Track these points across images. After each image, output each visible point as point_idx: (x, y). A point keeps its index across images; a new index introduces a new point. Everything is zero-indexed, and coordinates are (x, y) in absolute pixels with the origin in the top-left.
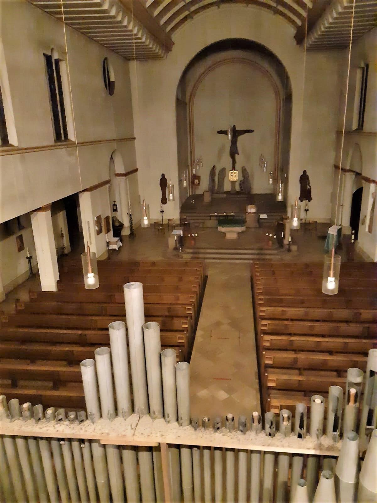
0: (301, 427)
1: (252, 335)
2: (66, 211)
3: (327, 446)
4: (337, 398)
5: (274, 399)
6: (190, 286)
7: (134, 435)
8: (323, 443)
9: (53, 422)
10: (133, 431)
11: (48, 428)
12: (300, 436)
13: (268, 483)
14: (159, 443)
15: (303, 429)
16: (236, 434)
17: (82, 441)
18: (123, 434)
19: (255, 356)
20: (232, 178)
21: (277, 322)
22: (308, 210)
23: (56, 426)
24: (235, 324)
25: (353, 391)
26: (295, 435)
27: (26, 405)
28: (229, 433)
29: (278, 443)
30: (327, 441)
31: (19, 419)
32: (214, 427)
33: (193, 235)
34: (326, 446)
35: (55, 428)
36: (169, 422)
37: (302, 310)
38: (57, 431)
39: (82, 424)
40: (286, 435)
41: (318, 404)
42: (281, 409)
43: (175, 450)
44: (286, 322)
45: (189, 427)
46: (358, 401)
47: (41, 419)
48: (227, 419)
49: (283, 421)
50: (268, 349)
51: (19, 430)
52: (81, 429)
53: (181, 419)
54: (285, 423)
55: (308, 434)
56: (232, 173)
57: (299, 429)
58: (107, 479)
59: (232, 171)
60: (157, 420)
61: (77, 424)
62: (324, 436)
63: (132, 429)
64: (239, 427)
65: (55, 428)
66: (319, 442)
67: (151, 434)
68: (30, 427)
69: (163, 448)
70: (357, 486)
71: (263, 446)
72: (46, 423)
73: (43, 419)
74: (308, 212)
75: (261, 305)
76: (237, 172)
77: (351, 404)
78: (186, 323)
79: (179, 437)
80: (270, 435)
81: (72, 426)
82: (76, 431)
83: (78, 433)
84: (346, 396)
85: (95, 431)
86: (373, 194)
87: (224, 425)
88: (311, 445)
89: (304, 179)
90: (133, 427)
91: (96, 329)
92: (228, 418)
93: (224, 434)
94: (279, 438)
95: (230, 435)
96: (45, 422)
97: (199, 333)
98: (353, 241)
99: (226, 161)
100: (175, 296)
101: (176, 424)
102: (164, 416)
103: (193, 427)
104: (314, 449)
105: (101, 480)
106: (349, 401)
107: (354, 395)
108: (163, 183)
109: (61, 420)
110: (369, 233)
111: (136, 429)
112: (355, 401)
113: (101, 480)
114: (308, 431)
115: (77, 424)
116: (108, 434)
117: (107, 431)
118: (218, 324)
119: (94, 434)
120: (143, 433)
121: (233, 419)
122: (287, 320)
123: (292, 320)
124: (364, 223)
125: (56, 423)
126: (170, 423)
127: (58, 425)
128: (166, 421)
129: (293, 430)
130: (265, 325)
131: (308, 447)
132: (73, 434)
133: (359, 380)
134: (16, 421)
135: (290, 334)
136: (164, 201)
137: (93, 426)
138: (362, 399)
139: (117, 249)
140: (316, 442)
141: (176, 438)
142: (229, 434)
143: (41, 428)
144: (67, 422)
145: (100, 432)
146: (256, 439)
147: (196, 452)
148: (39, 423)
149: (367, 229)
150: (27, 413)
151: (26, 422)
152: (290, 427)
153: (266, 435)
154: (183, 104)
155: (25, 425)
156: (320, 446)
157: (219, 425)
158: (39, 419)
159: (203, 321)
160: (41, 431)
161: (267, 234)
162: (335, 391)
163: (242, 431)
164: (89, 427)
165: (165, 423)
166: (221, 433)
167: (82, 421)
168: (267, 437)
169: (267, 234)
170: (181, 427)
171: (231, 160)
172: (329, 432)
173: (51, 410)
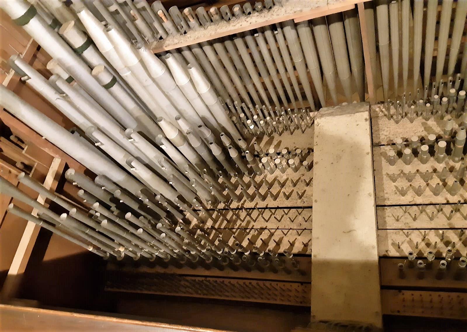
5: (357, 112)
6: (454, 83)
9: (243, 18)
11: (240, 24)
17: (273, 27)
18: (317, 6)
23: (248, 20)
27: (186, 11)
31: (211, 25)
35: (247, 22)
38: (251, 23)
39: (271, 11)
42: (302, 165)
46: (267, 116)
47: (230, 18)
51: (216, 33)
52: (272, 14)
58: (303, 58)
61: (266, 12)
65: (247, 22)
68: (224, 28)
72: (237, 20)
73: (232, 18)
81: (263, 15)
82: (268, 18)
83: (271, 19)
85: (287, 12)
91: (425, 9)
96: (235, 20)
105: (298, 60)
109: (250, 13)
113: (298, 60)
115: (266, 12)
116: (301, 11)
117: (299, 9)
119: (288, 15)
125: (246, 17)
127: (249, 18)
132: (267, 21)
134: (209, 27)
137: (283, 10)
143: (235, 26)
144: (256, 14)
145: (292, 11)
147: (228, 43)
148: (230, 22)
150: (216, 17)
151: (218, 25)
155: (219, 27)
158: (229, 19)
160: (236, 28)
164: (280, 11)
167: (271, 8)
173: (237, 7)
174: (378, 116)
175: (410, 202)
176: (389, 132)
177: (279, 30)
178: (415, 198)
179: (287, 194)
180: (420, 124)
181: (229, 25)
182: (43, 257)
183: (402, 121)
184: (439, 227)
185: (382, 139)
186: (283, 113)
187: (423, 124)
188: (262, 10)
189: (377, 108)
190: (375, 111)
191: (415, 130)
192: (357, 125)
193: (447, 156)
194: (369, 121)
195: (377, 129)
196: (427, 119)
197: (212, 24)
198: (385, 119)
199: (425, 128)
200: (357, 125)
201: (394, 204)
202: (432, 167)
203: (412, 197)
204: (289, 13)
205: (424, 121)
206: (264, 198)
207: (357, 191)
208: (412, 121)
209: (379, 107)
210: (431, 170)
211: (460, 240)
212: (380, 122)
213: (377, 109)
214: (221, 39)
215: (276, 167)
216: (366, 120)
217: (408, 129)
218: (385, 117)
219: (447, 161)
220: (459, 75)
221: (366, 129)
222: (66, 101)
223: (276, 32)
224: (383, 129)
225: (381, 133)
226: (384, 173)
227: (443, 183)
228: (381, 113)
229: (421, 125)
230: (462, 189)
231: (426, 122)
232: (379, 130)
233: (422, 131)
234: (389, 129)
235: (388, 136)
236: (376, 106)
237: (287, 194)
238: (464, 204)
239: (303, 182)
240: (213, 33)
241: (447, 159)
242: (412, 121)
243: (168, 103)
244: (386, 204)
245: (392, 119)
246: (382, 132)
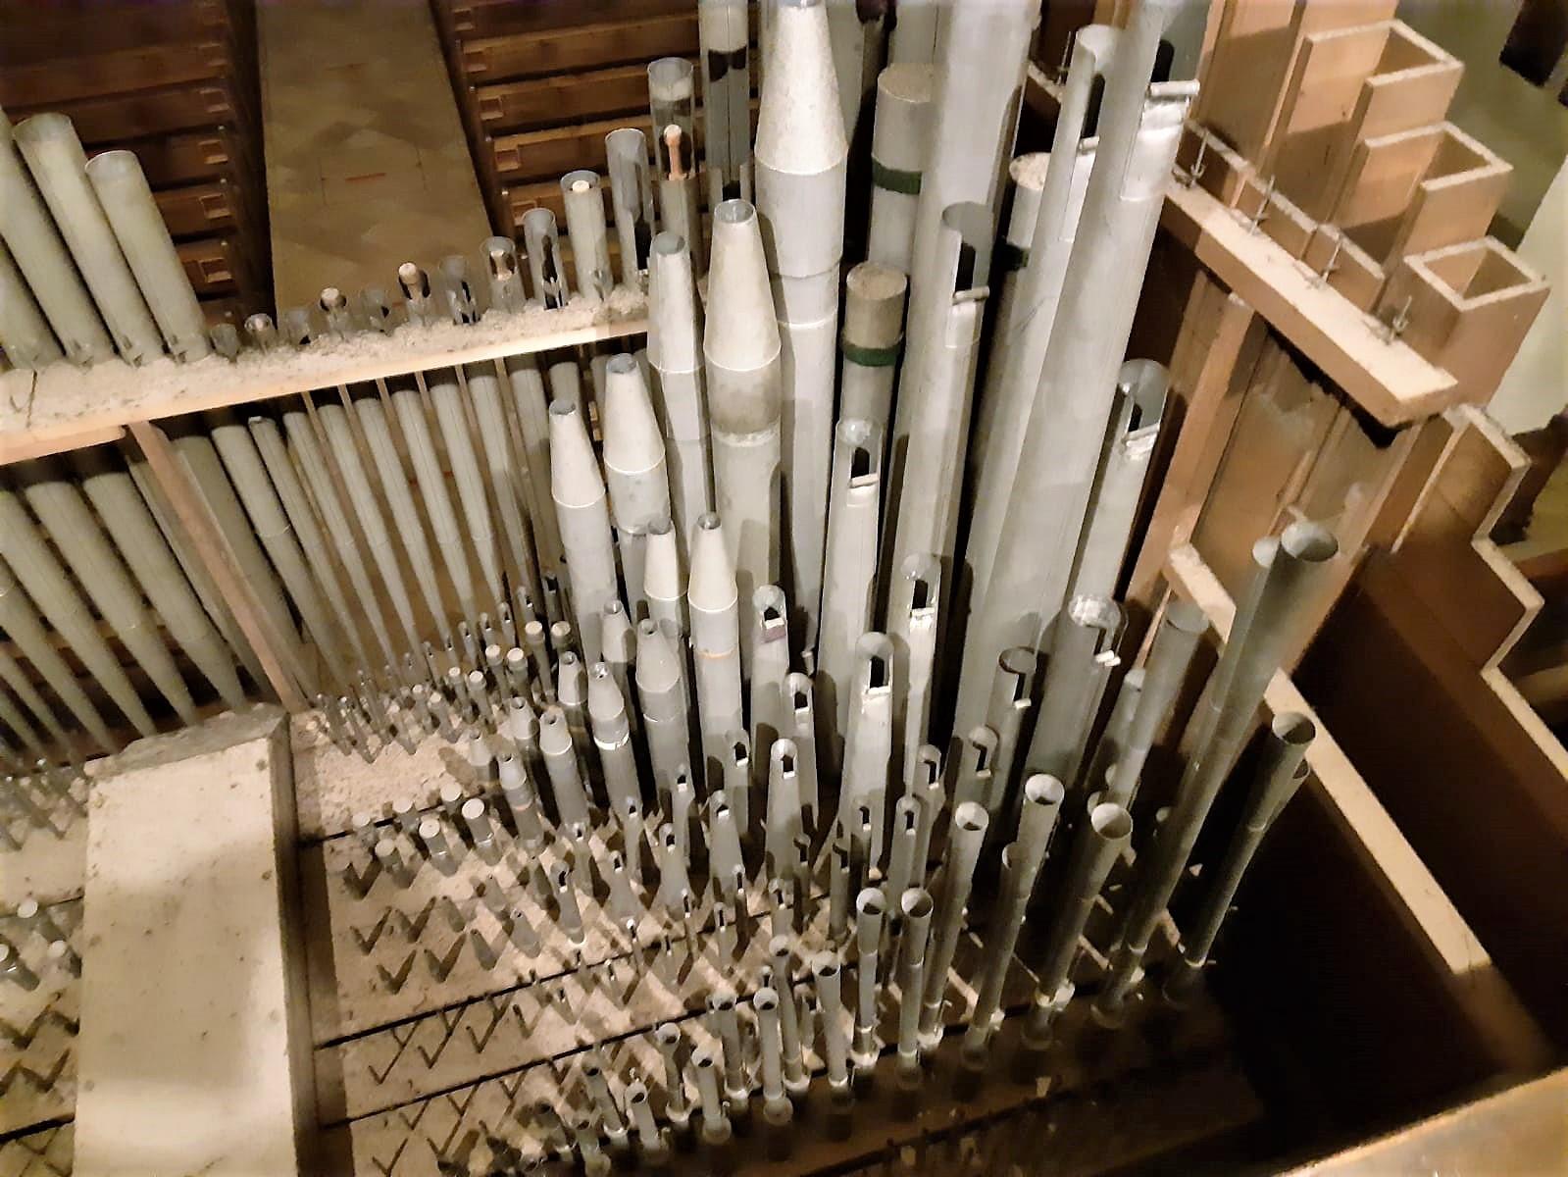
0: (550, 272)
1: (459, 150)
3: (629, 310)
4: (633, 169)
7: (29, 424)
8: (616, 305)
10: (23, 417)
12: (551, 304)
13: (499, 461)
14: (126, 427)
15: (555, 279)
16: (365, 341)
19: (482, 211)
21: (526, 87)
24: (398, 123)
25: (673, 132)
26: (538, 304)
28: (341, 346)
29: (492, 336)
30: (624, 300)
32: (290, 342)
34: (625, 312)
36: (138, 361)
37: (602, 30)
40: (511, 308)
41: (583, 194)
43: (193, 444)
44: (557, 82)
45: (210, 360)
48: (325, 308)
49: (495, 271)
50: (515, 182)
53: (176, 341)
54: (500, 277)
55: (575, 294)
57: (543, 282)
60: (97, 368)
62: (618, 288)
63: (19, 411)
64: (368, 322)
66: (606, 306)
67: (88, 406)
69: (150, 443)
70: (703, 376)
71: (451, 351)
75: (466, 37)
77: (676, 175)
78: (215, 150)
79: (183, 392)
80: (466, 319)
84: (655, 157)
87: (321, 328)
88: (587, 317)
90: (18, 405)
92: (326, 303)
93: (325, 351)
94: (492, 321)
95: (346, 349)
97: (277, 177)
100: (143, 58)
101: (166, 361)
102: (117, 351)
103: (224, 355)
104: (594, 325)
106: (667, 168)
107: (678, 142)
111: (30, 408)
112: (685, 167)
114: (573, 286)
118: (338, 135)
120: (58, 411)
121: (343, 301)
122: (558, 73)
123: (578, 71)
126: (145, 365)
128: (129, 364)
129: (529, 292)
130: (492, 105)
131: (577, 325)
133: (682, 89)
135: (578, 121)
138: (701, 155)
140: (596, 309)
141: (176, 397)
142: (341, 347)
146: (426, 340)
152: (518, 285)
153: (455, 323)
156: (611, 317)
157: (306, 330)
159: (280, 139)
162: (624, 143)
163: (382, 331)
165: (125, 366)
166: (315, 352)
168: (457, 327)
170: (185, 366)
172: (631, 272)
174: (314, 748)
175: (415, 1008)
176: (346, 791)
178: (429, 993)
179: (441, 958)
180: (436, 753)
183: (383, 752)
184: (499, 1068)
185: (327, 817)
186: (41, 762)
187: (443, 753)
189: (308, 723)
190: (303, 732)
191: (423, 775)
192: (233, 787)
193: (510, 837)
194: (268, 768)
195: (313, 788)
196: (454, 738)
198: (335, 753)
199: (449, 766)
200: (233, 787)
201: (367, 1026)
202: (472, 880)
203: (420, 989)
205: (445, 743)
206: (443, 970)
207: (233, 1015)
208: (411, 750)
209: (316, 719)
210: (469, 891)
211: (561, 1091)
212: (321, 764)
213: (311, 726)
215: (426, 855)
216: (261, 766)
217: (402, 775)
218: (334, 747)
219: (512, 854)
220: (463, 625)
221: (262, 797)
224: (330, 785)
225: (322, 801)
226: (336, 925)
227: (504, 923)
228: (321, 735)
229: (438, 757)
230: (556, 929)
231: (452, 746)
232: (315, 790)
233: (442, 775)
234: (346, 782)
235: (344, 806)
236: (306, 716)
237: (441, 958)
238: (564, 978)
239: (351, 936)
241: (511, 849)
242: (411, 750)
244: (346, 1033)
245: (354, 751)
246: (327, 797)
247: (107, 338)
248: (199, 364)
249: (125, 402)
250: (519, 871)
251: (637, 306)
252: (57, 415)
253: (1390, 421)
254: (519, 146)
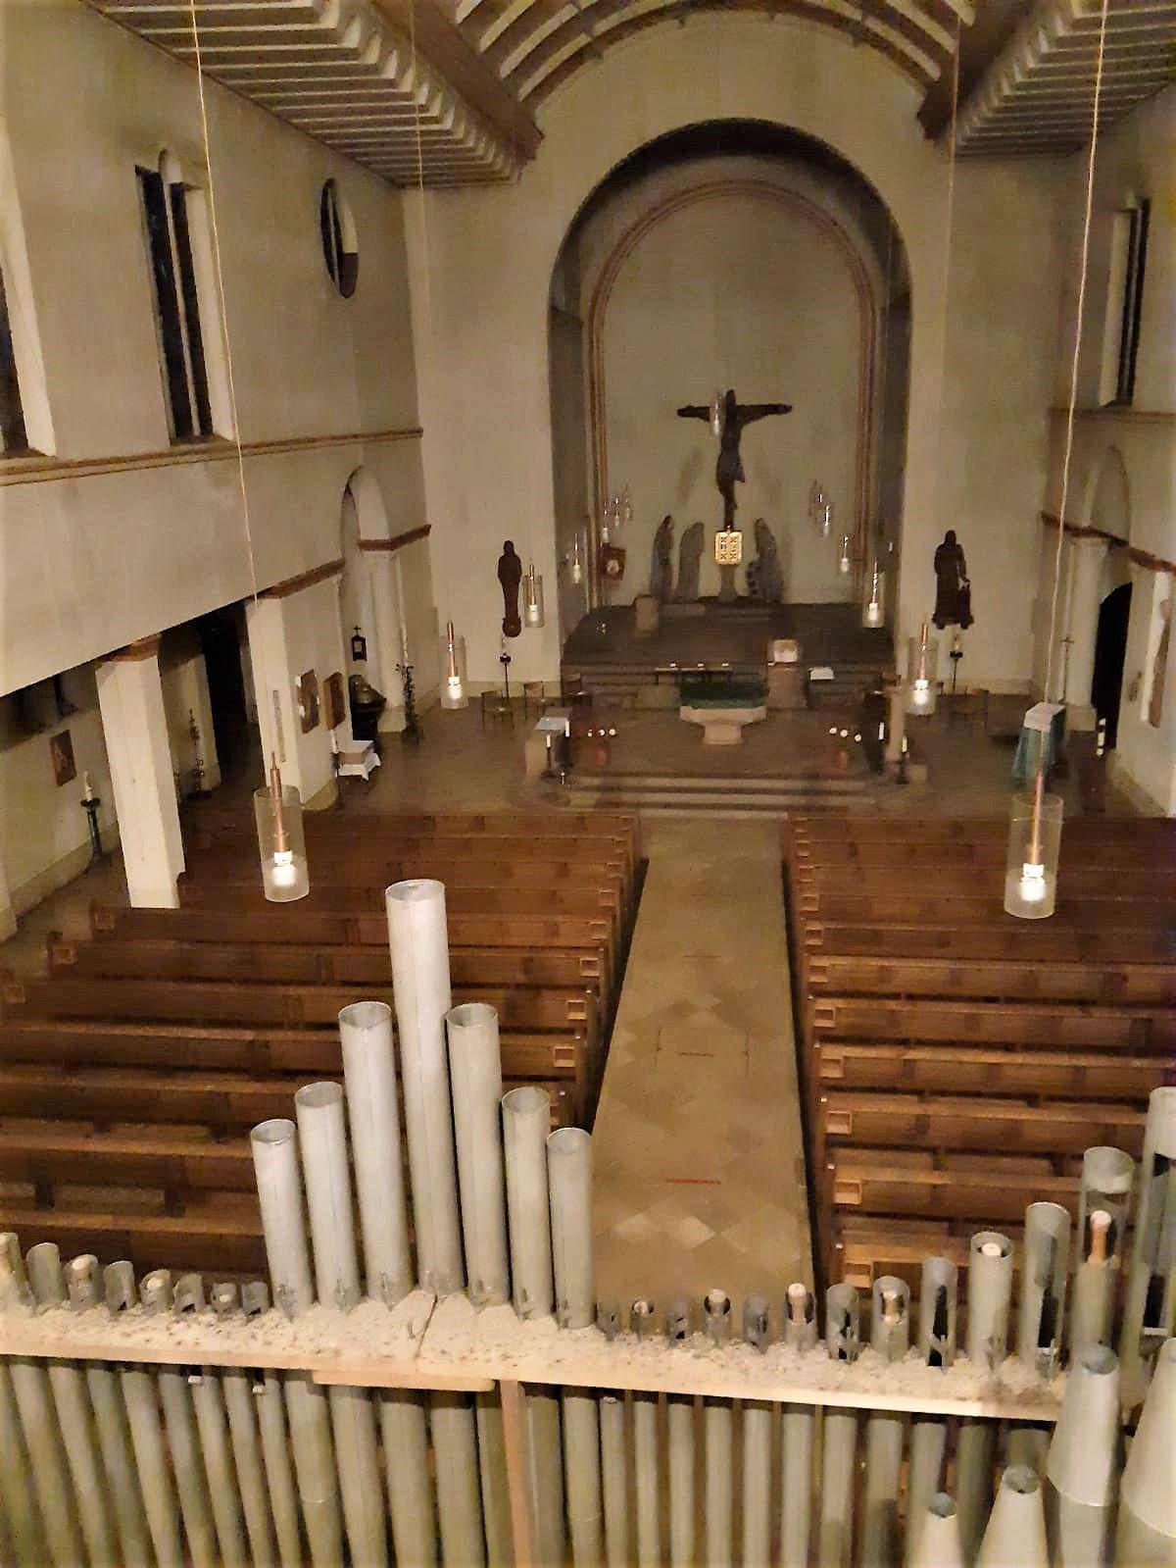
0: (940, 1330)
1: (786, 1044)
2: (206, 658)
3: (1021, 1391)
4: (1050, 1241)
7: (417, 1355)
8: (1007, 1380)
9: (165, 1317)
10: (414, 1343)
11: (148, 1335)
12: (935, 1360)
14: (497, 1382)
15: (946, 1337)
17: (255, 1375)
18: (385, 1353)
19: (796, 1108)
20: (723, 556)
21: (863, 1004)
22: (960, 655)
23: (176, 1328)
24: (733, 1010)
25: (1101, 1219)
26: (921, 1355)
28: (713, 1351)
29: (867, 1381)
30: (1019, 1375)
31: (58, 1307)
32: (667, 1332)
33: (602, 732)
34: (1017, 1390)
35: (171, 1334)
36: (526, 1316)
37: (942, 966)
38: (179, 1343)
40: (892, 1356)
44: (892, 1005)
45: (590, 1331)
47: (128, 1305)
50: (836, 1088)
51: (60, 1339)
52: (254, 1337)
53: (566, 1306)
54: (888, 1319)
56: (724, 539)
57: (931, 1336)
58: (334, 1492)
59: (723, 534)
60: (489, 1310)
61: (240, 1322)
62: (1010, 1360)
63: (412, 1337)
64: (745, 1331)
65: (171, 1334)
66: (995, 1378)
67: (472, 1352)
68: (93, 1331)
69: (509, 1398)
70: (1114, 1515)
71: (821, 1389)
72: (144, 1317)
73: (133, 1307)
74: (960, 659)
75: (814, 951)
76: (740, 537)
77: (1096, 1258)
78: (579, 1007)
79: (558, 1361)
80: (842, 1355)
81: (225, 1327)
82: (238, 1342)
83: (243, 1350)
84: (1079, 1234)
85: (297, 1343)
86: (1163, 604)
87: (698, 1324)
88: (970, 1387)
89: (949, 557)
90: (414, 1332)
92: (711, 1304)
93: (698, 1352)
94: (869, 1364)
95: (718, 1357)
97: (620, 1038)
98: (1100, 752)
99: (706, 501)
100: (545, 922)
101: (550, 1320)
102: (511, 1297)
103: (603, 1331)
104: (980, 1399)
105: (315, 1497)
106: (1088, 1249)
107: (1105, 1230)
108: (510, 569)
109: (189, 1309)
110: (1151, 727)
111: (423, 1336)
112: (1109, 1251)
113: (315, 1497)
114: (962, 1342)
115: (240, 1322)
116: (337, 1353)
117: (333, 1345)
118: (680, 1010)
119: (295, 1352)
120: (446, 1349)
121: (727, 1307)
122: (896, 996)
123: (911, 997)
124: (1134, 694)
125: (174, 1318)
126: (531, 1320)
128: (517, 1314)
129: (913, 1339)
130: (825, 1014)
131: (960, 1392)
132: (229, 1352)
133: (1119, 1184)
136: (512, 626)
138: (1128, 1244)
139: (365, 776)
140: (985, 1379)
141: (550, 1365)
142: (715, 1352)
143: (128, 1335)
144: (210, 1317)
145: (311, 1347)
146: (799, 1369)
148: (123, 1317)
149: (1144, 715)
150: (84, 1289)
151: (80, 1314)
152: (904, 1332)
153: (831, 1357)
154: (570, 326)
155: (79, 1324)
156: (997, 1392)
157: (684, 1326)
158: (123, 1307)
159: (632, 1002)
160: (128, 1343)
161: (833, 730)
162: (1045, 1218)
163: (754, 1344)
164: (279, 1331)
167: (256, 1312)
168: (832, 1361)
169: (833, 730)
170: (566, 1331)
171: (719, 500)
172: (1027, 1346)
173: (158, 1278)
177: (271, 1384)
181: (114, 1327)
182: (208, 664)
188: (230, 1308)
197: (64, 1303)
204: (301, 1347)
214: (265, 1266)
222: (384, 64)
223: (257, 1389)
240: (52, 1335)
243: (539, 1206)
247: (597, 1431)
248: (578, 1333)
249: (505, 1357)
250: (203, 1370)
251: (1031, 1388)
252: (443, 1352)
253: (1127, 215)
254: (846, 1058)
